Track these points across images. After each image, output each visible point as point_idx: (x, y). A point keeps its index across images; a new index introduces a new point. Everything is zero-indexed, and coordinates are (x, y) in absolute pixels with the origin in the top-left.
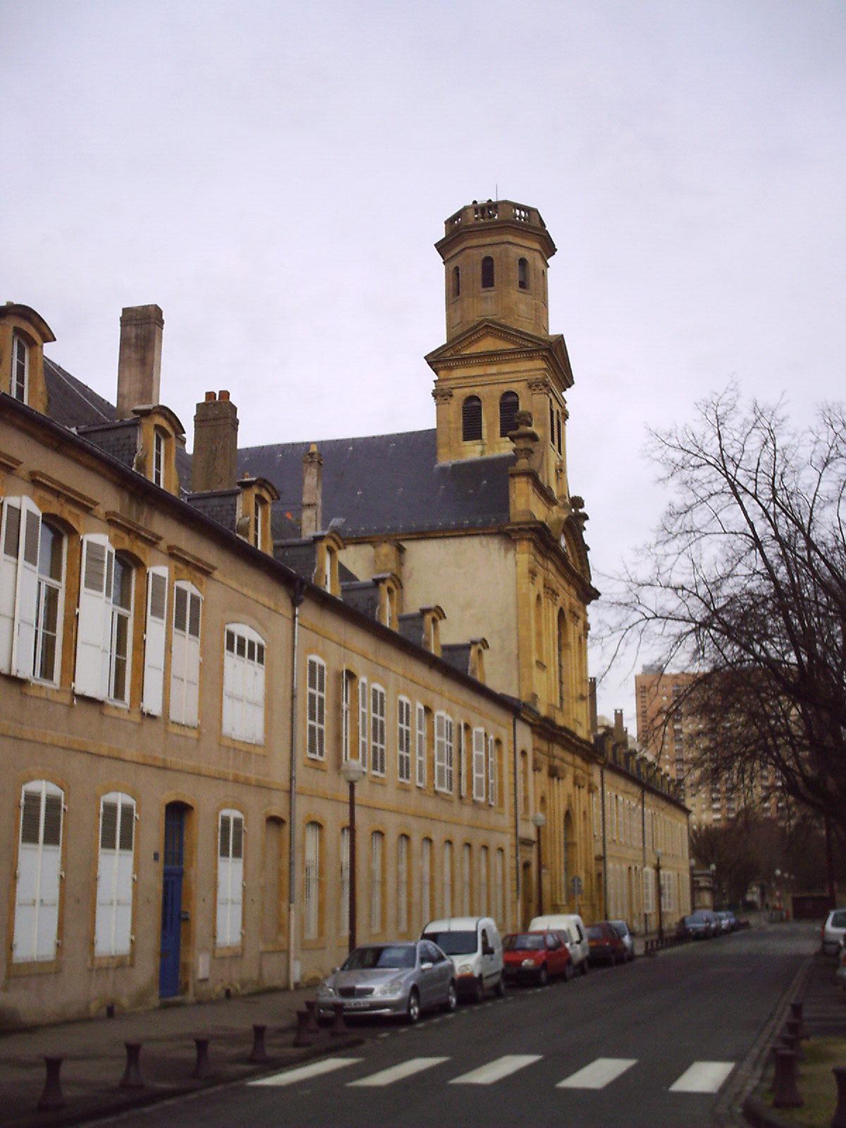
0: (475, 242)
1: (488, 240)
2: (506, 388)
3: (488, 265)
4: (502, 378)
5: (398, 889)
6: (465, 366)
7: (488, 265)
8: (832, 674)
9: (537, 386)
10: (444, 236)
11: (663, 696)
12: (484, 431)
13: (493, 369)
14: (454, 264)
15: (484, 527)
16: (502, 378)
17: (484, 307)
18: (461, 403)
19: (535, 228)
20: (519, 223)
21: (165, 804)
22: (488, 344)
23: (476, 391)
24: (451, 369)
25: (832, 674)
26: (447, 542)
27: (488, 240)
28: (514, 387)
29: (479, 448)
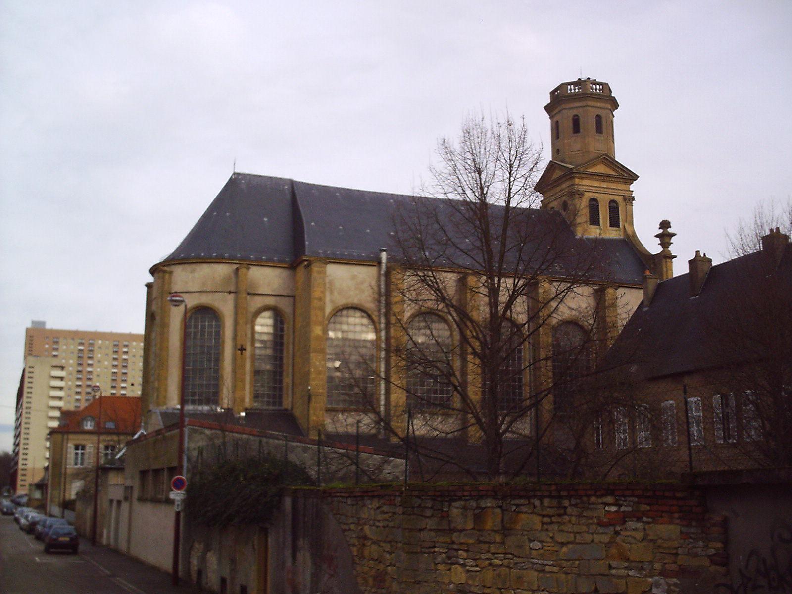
0: (590, 104)
1: (599, 105)
2: (612, 197)
3: (576, 122)
4: (611, 191)
5: (336, 453)
6: (590, 179)
7: (576, 122)
8: (280, 434)
9: (629, 200)
10: (550, 102)
11: (63, 359)
12: (601, 221)
13: (605, 185)
14: (555, 119)
15: (267, 261)
16: (611, 191)
17: (574, 144)
18: (588, 200)
19: (607, 96)
20: (596, 94)
21: (39, 318)
22: (601, 169)
23: (596, 196)
24: (582, 178)
25: (280, 434)
26: (633, 290)
27: (599, 105)
28: (616, 198)
29: (598, 231)
